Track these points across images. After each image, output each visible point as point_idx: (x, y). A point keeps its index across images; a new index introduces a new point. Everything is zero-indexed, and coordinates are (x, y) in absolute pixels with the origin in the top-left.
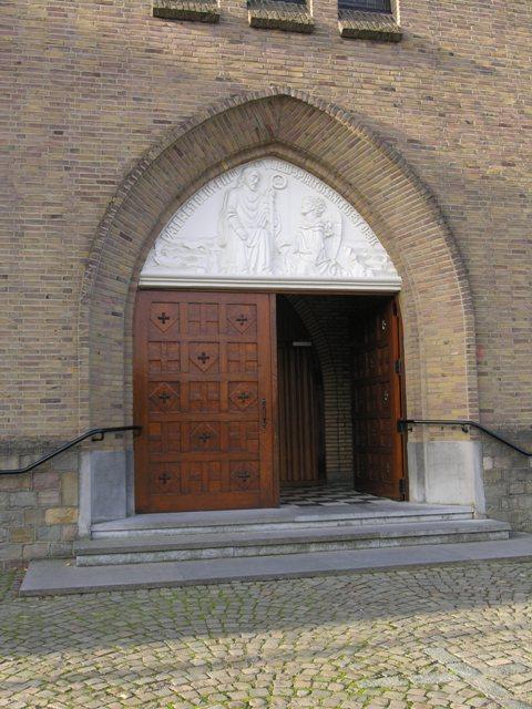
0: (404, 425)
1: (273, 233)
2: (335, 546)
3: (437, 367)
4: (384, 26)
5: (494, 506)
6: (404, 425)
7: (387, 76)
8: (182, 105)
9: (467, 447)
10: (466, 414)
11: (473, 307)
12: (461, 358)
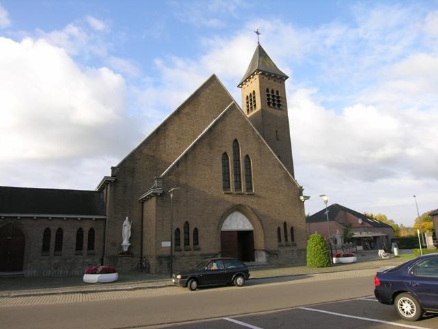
0: (254, 250)
1: (237, 223)
2: (32, 297)
3: (259, 242)
4: (251, 193)
5: (268, 262)
6: (254, 250)
7: (252, 200)
8: (228, 206)
9: (264, 253)
10: (264, 249)
11: (264, 233)
12: (263, 240)
